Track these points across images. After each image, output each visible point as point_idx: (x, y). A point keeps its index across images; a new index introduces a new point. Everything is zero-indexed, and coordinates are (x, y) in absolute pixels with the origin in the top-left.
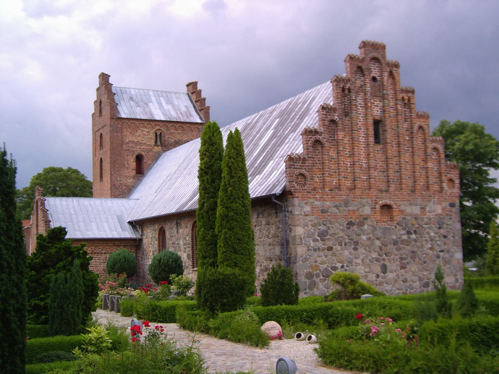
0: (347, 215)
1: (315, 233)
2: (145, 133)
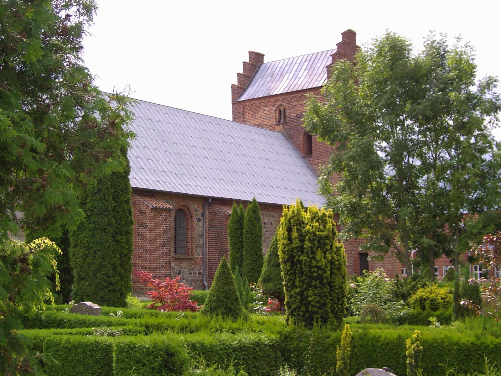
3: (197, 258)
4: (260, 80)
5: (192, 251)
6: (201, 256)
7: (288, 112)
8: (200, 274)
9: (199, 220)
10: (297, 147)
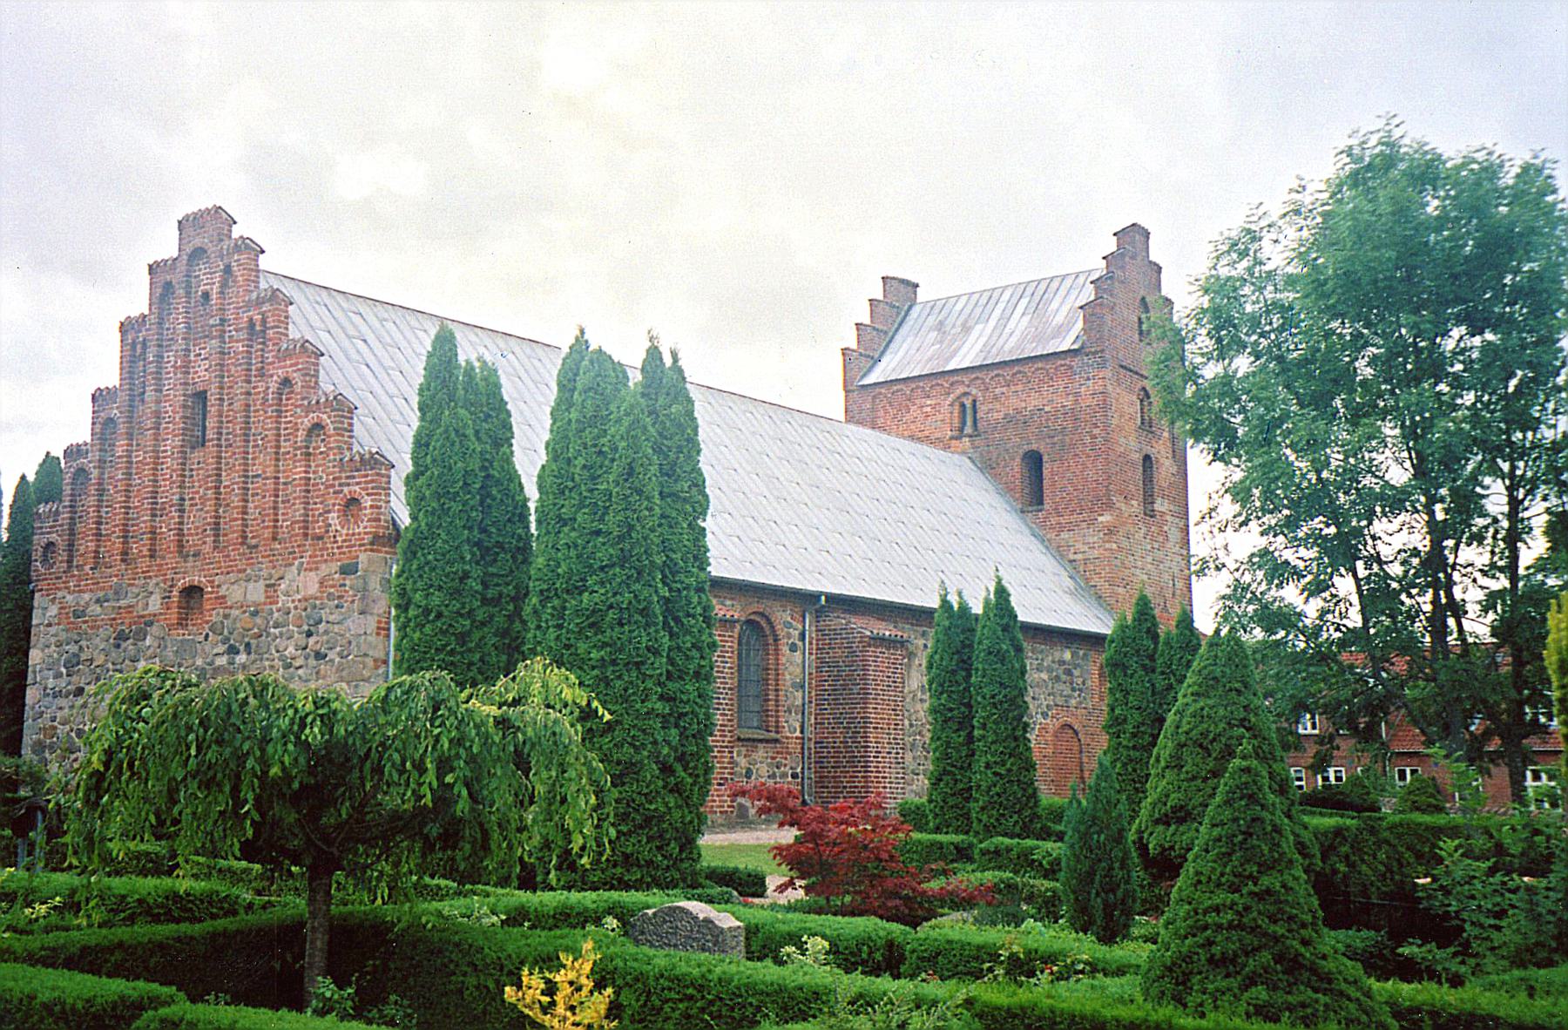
0: (114, 619)
1: (59, 660)
2: (929, 409)
3: (787, 738)
4: (909, 340)
5: (777, 722)
6: (798, 734)
7: (982, 409)
8: (794, 776)
9: (793, 648)
10: (1007, 489)
